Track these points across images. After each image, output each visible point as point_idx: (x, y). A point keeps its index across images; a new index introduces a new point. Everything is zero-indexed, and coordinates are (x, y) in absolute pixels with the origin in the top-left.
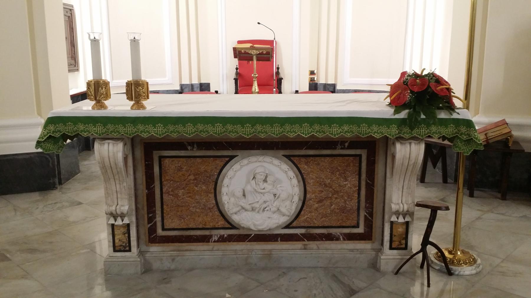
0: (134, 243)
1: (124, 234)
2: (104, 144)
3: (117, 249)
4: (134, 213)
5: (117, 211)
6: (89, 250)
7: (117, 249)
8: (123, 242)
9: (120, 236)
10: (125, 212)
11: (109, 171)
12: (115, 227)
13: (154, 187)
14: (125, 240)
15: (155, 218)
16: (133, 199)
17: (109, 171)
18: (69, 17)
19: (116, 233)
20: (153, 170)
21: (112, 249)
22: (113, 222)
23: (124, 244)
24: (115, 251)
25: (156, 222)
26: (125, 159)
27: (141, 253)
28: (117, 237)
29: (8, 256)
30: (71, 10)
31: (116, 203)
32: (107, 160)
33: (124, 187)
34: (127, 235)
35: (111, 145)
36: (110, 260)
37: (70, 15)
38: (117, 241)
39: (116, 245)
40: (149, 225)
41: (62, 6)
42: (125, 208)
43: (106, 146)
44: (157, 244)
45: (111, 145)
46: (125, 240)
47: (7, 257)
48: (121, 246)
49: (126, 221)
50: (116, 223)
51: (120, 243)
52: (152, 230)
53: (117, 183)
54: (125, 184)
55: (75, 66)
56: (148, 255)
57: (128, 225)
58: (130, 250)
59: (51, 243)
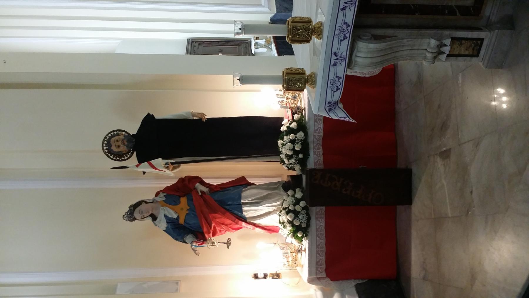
0: (475, 35)
1: (461, 44)
2: (355, 61)
3: (475, 53)
4: (440, 32)
5: (434, 51)
6: (460, 74)
7: (475, 53)
8: (471, 46)
9: (463, 49)
10: (438, 43)
11: (386, 58)
12: (451, 53)
13: (413, 5)
14: (469, 44)
15: (451, 7)
16: (423, 31)
17: (386, 58)
18: (199, 44)
19: (457, 53)
20: (393, 5)
21: (474, 59)
22: (445, 56)
23: (473, 45)
24: (477, 56)
25: (457, 6)
26: (376, 38)
27: (489, 26)
28: (463, 52)
29: (444, 149)
30: (192, 42)
31: (425, 51)
32: (375, 60)
33: (408, 41)
34: (463, 42)
35: (359, 54)
36: (486, 61)
37: (197, 44)
38: (467, 53)
39: (471, 53)
40: (458, 14)
41: (189, 55)
42: (433, 42)
43: (358, 60)
44: (484, 7)
45: (359, 54)
46: (469, 44)
47: (446, 151)
48: (473, 49)
49: (448, 42)
50: (447, 53)
51: (471, 50)
52: (465, 11)
53: (401, 49)
54: (406, 40)
55: (247, 43)
56: (493, 19)
57: (453, 39)
58: (482, 40)
59: (439, 106)
